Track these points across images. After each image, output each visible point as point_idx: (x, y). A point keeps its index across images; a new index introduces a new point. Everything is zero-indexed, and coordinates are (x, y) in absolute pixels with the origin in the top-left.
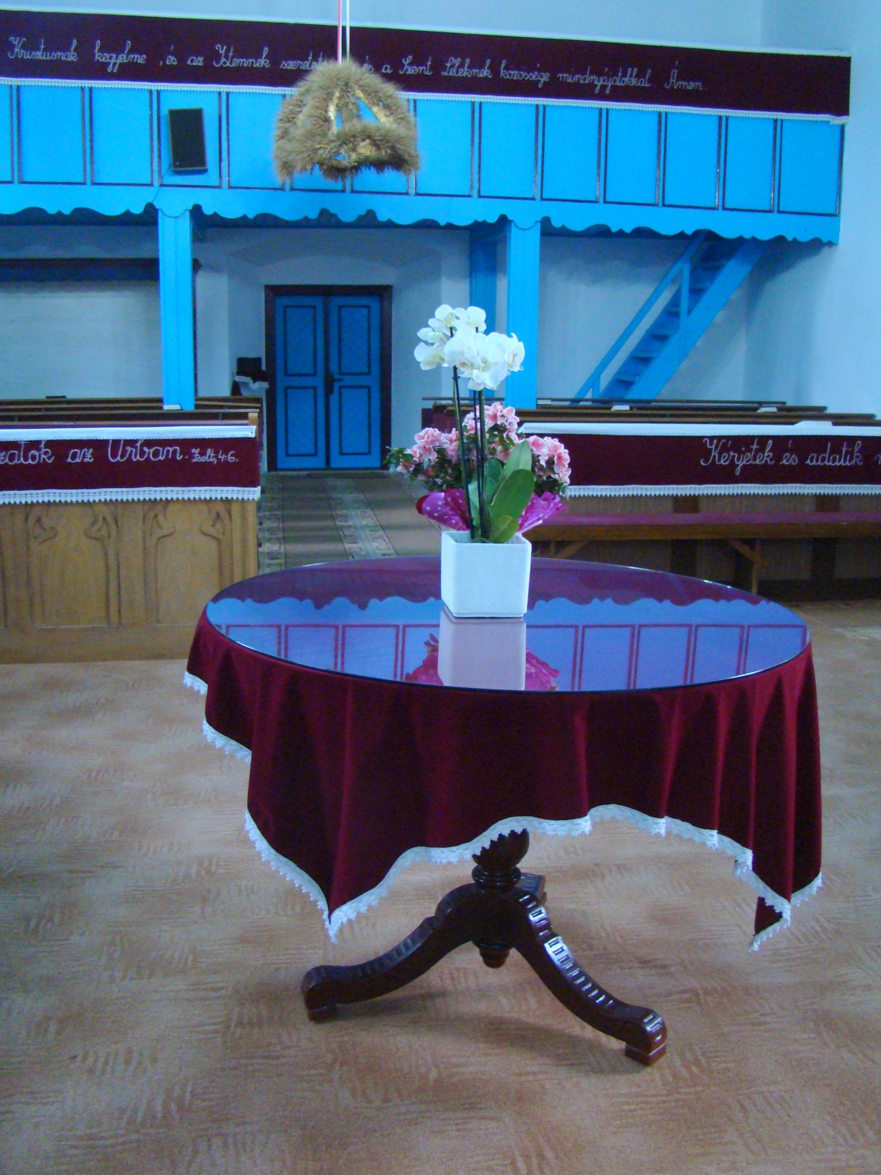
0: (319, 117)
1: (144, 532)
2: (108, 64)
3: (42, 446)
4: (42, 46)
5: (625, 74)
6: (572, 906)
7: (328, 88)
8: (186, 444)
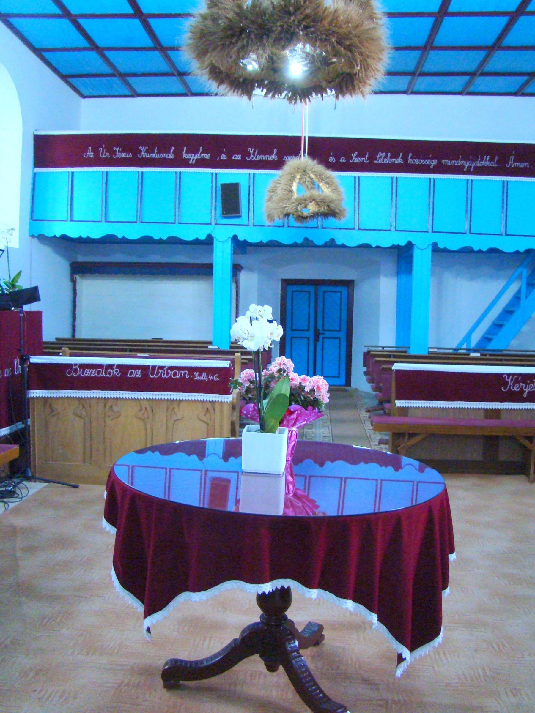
0: (287, 190)
1: (167, 416)
2: (190, 159)
3: (115, 367)
4: (156, 151)
5: (482, 160)
6: (339, 644)
7: (292, 174)
8: (192, 370)
